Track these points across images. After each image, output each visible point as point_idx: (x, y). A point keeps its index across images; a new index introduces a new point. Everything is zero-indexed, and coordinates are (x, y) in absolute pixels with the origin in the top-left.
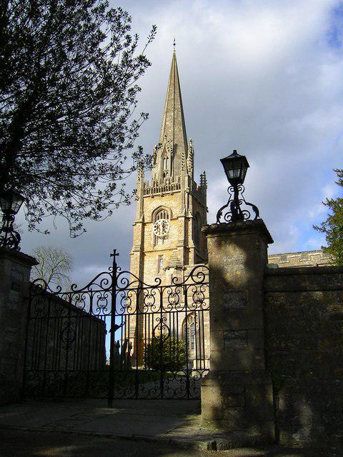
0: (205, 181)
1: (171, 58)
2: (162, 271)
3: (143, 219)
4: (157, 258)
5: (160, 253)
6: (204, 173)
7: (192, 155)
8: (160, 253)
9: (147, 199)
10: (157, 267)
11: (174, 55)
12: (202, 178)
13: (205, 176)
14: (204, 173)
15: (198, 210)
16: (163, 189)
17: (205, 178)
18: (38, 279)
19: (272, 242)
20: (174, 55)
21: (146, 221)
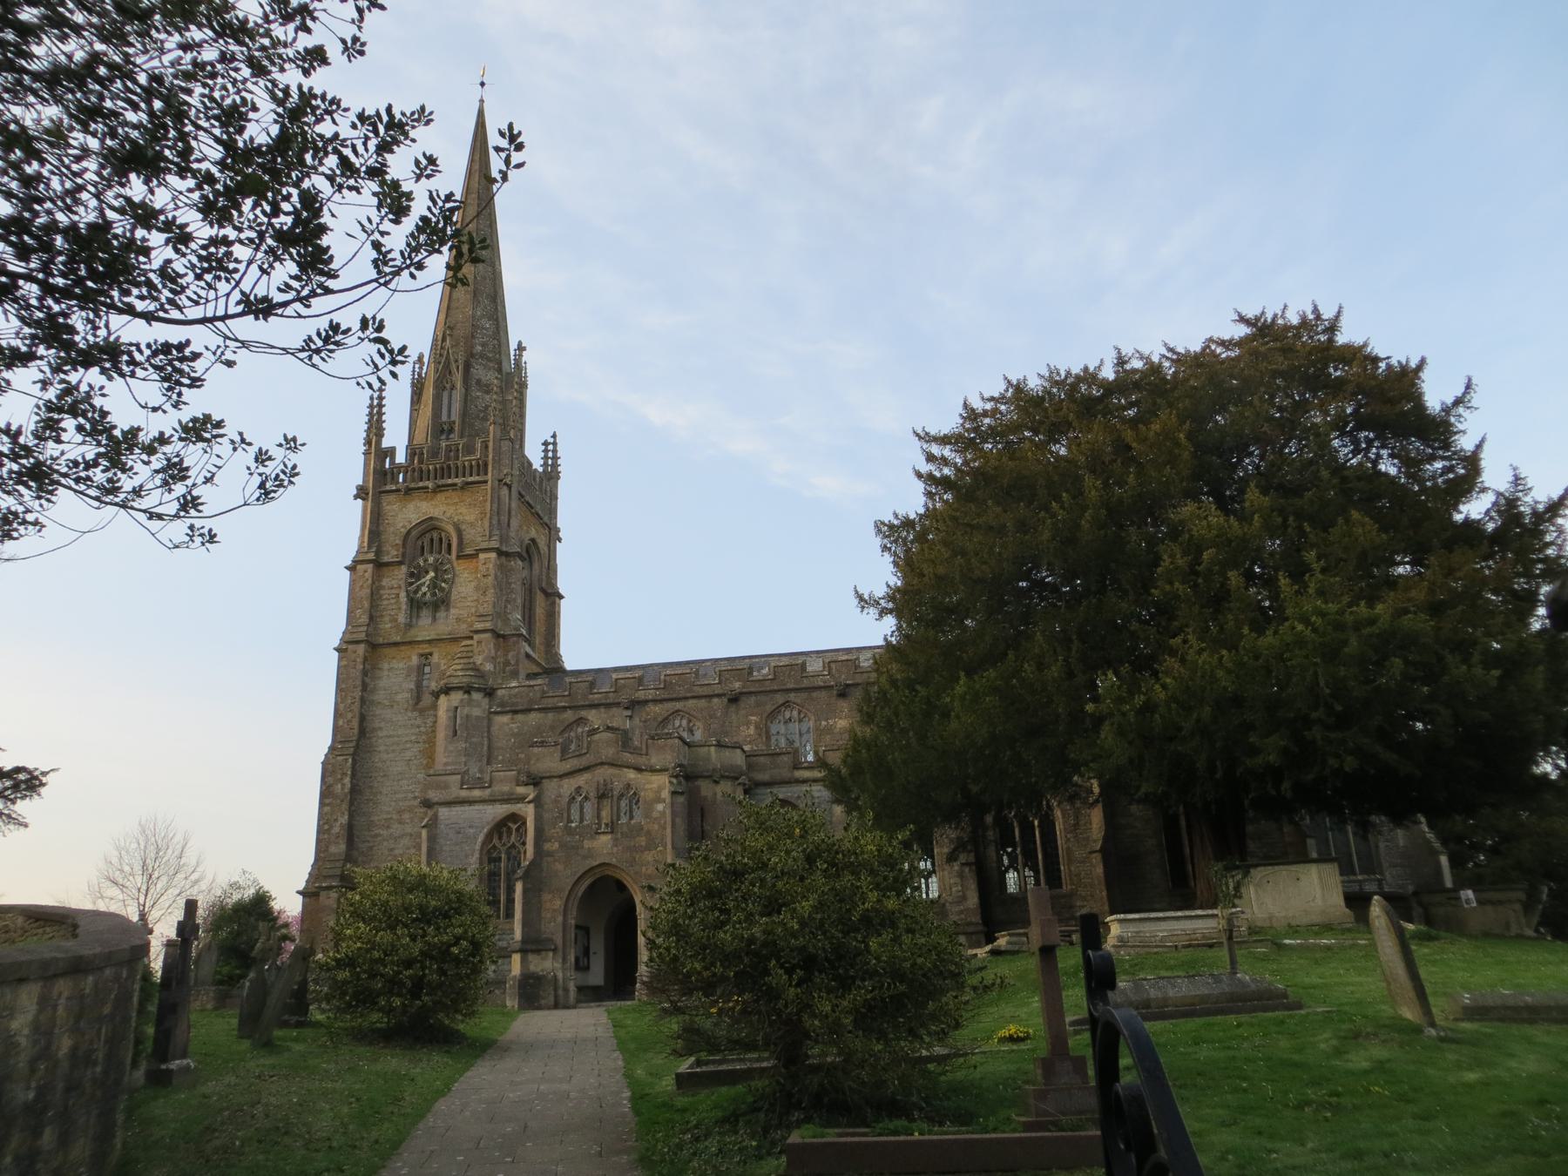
0: (555, 458)
1: (1336, 310)
2: (427, 699)
3: (378, 553)
4: (415, 660)
5: (426, 649)
6: (554, 436)
7: (368, 364)
8: (426, 649)
9: (392, 497)
10: (412, 686)
11: (481, 114)
12: (546, 451)
13: (555, 444)
14: (554, 436)
15: (533, 533)
16: (445, 472)
17: (555, 451)
18: (561, 777)
19: (561, 597)
20: (481, 114)
21: (386, 559)
